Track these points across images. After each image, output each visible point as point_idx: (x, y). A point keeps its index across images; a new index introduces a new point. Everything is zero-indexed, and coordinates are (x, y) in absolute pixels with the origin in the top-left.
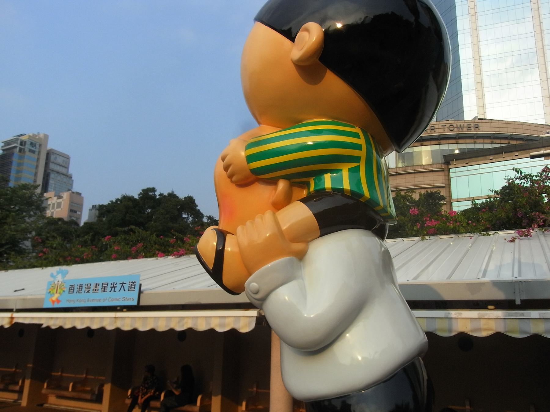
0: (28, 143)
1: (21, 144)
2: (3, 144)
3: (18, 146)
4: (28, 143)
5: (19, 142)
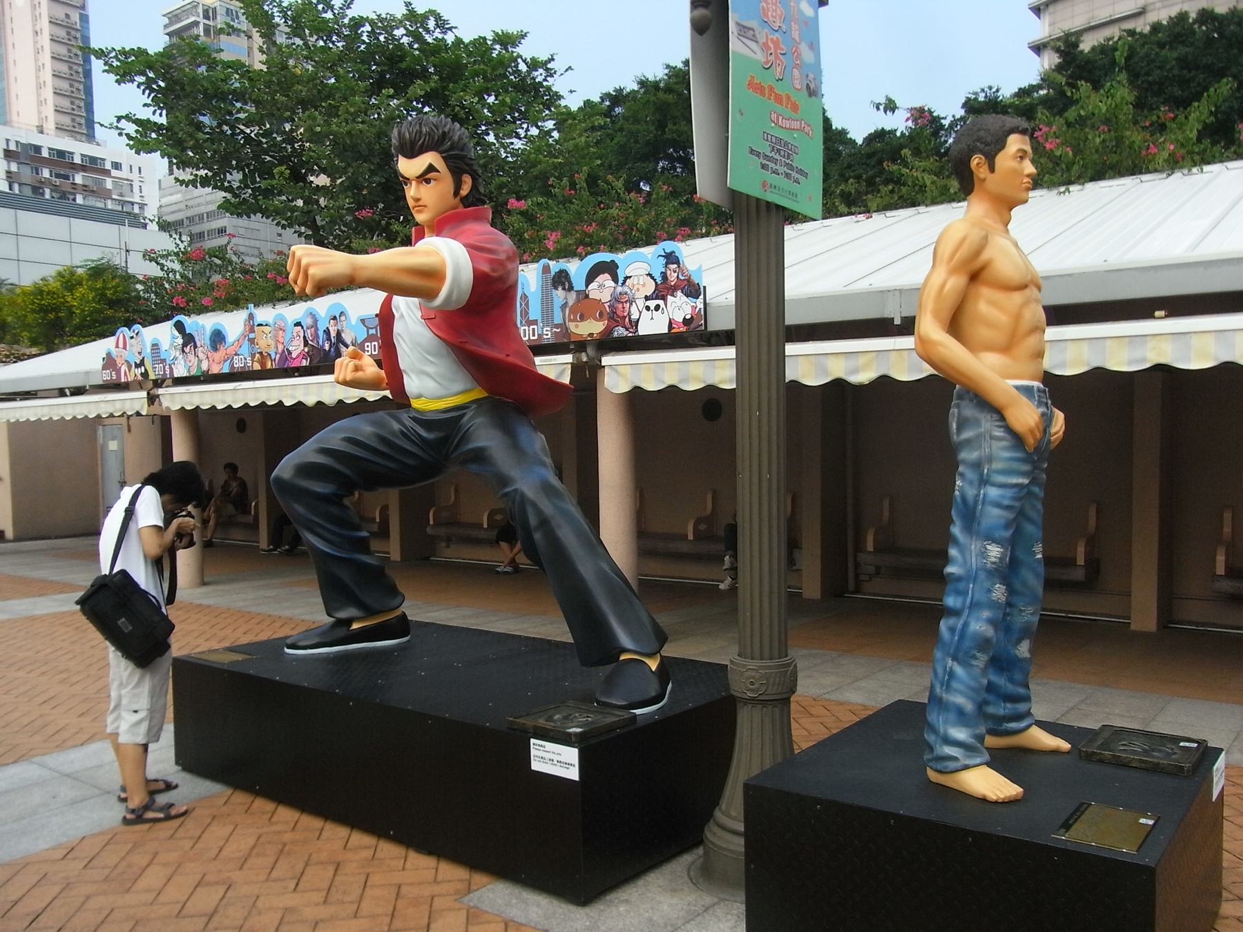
0: (221, 12)
1: (206, 17)
2: (166, 21)
3: (203, 21)
4: (221, 12)
5: (200, 11)
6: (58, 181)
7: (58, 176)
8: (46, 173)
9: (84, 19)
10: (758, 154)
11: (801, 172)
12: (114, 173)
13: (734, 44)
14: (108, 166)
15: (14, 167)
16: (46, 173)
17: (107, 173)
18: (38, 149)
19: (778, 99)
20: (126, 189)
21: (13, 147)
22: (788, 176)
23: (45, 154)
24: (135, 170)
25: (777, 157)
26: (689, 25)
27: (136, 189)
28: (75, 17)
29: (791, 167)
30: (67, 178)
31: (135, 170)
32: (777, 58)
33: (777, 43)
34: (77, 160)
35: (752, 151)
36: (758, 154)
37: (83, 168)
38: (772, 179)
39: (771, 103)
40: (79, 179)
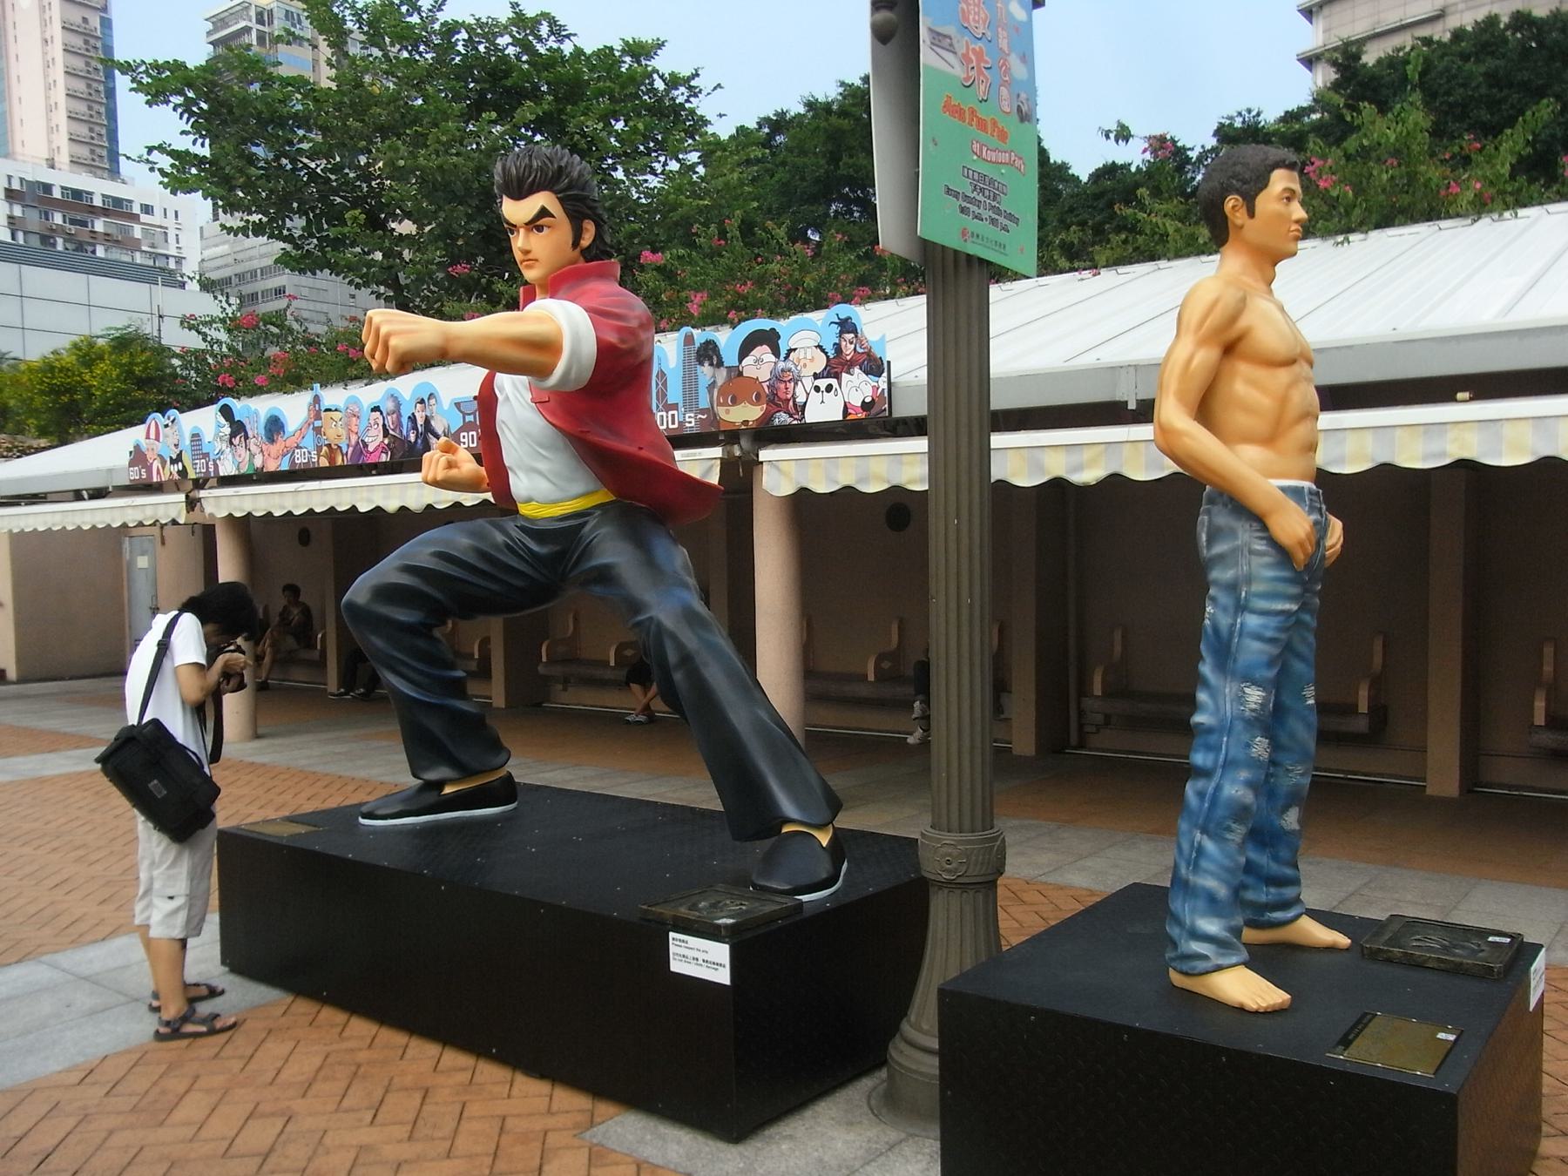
0: (279, 15)
1: (260, 21)
2: (210, 26)
3: (255, 27)
4: (279, 15)
5: (253, 13)
6: (73, 229)
7: (73, 222)
8: (58, 219)
9: (107, 24)
10: (956, 195)
11: (1010, 217)
12: (144, 218)
13: (927, 56)
14: (136, 210)
15: (18, 211)
16: (58, 219)
17: (135, 218)
18: (47, 188)
19: (982, 125)
20: (159, 239)
21: (16, 186)
22: (993, 222)
23: (57, 194)
24: (171, 214)
25: (980, 198)
26: (869, 31)
27: (172, 239)
28: (95, 21)
29: (998, 211)
30: (84, 224)
31: (171, 214)
32: (980, 73)
33: (980, 55)
34: (97, 202)
35: (948, 191)
36: (956, 195)
37: (105, 212)
38: (973, 225)
39: (973, 129)
40: (99, 225)
